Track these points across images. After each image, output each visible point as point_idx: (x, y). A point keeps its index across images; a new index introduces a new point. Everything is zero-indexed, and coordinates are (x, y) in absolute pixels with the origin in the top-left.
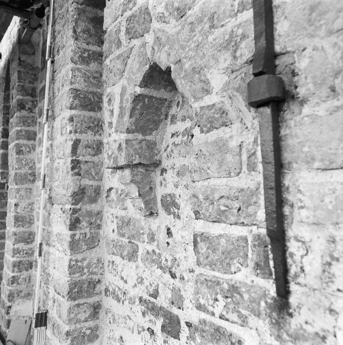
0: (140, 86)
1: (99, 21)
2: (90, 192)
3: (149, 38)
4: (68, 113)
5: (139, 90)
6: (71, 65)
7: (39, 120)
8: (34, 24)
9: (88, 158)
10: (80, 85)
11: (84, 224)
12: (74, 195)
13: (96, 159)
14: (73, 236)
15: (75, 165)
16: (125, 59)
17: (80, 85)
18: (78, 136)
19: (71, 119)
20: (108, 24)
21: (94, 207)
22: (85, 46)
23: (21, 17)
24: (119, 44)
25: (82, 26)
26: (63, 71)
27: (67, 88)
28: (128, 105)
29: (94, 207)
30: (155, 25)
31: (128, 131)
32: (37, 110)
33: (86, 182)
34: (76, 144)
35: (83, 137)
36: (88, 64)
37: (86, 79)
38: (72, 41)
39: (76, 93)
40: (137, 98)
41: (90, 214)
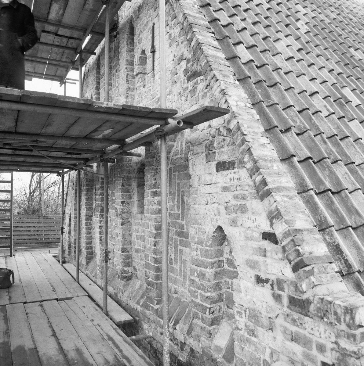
0: (335, 359)
1: (133, 39)
2: (131, 89)
3: (142, 44)
4: (125, 66)
5: (140, 55)
6: (126, 53)
7: (113, 78)
8: (112, 40)
9: (131, 79)
10: (129, 58)
11: (130, 97)
12: (127, 89)
13: (133, 80)
14: (127, 100)
15: (127, 81)
16: (138, 49)
17: (129, 58)
18: (128, 73)
19: (126, 68)
20: (135, 41)
21: (133, 93)
22: (130, 47)
23: (24, 79)
24: (137, 46)
25: (129, 41)
26: (124, 55)
27: (125, 59)
28: (139, 59)
29: (133, 93)
30: (143, 41)
31: (139, 65)
32: (112, 74)
33: (130, 86)
34: (127, 75)
35: (129, 73)
36: (131, 52)
37: (130, 56)
38: (126, 46)
39: (127, 61)
40: (140, 57)
41: (131, 95)
